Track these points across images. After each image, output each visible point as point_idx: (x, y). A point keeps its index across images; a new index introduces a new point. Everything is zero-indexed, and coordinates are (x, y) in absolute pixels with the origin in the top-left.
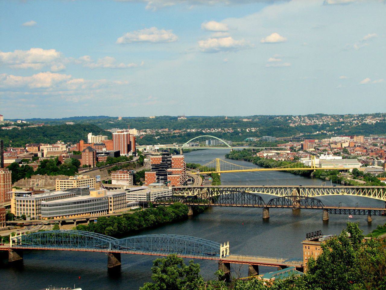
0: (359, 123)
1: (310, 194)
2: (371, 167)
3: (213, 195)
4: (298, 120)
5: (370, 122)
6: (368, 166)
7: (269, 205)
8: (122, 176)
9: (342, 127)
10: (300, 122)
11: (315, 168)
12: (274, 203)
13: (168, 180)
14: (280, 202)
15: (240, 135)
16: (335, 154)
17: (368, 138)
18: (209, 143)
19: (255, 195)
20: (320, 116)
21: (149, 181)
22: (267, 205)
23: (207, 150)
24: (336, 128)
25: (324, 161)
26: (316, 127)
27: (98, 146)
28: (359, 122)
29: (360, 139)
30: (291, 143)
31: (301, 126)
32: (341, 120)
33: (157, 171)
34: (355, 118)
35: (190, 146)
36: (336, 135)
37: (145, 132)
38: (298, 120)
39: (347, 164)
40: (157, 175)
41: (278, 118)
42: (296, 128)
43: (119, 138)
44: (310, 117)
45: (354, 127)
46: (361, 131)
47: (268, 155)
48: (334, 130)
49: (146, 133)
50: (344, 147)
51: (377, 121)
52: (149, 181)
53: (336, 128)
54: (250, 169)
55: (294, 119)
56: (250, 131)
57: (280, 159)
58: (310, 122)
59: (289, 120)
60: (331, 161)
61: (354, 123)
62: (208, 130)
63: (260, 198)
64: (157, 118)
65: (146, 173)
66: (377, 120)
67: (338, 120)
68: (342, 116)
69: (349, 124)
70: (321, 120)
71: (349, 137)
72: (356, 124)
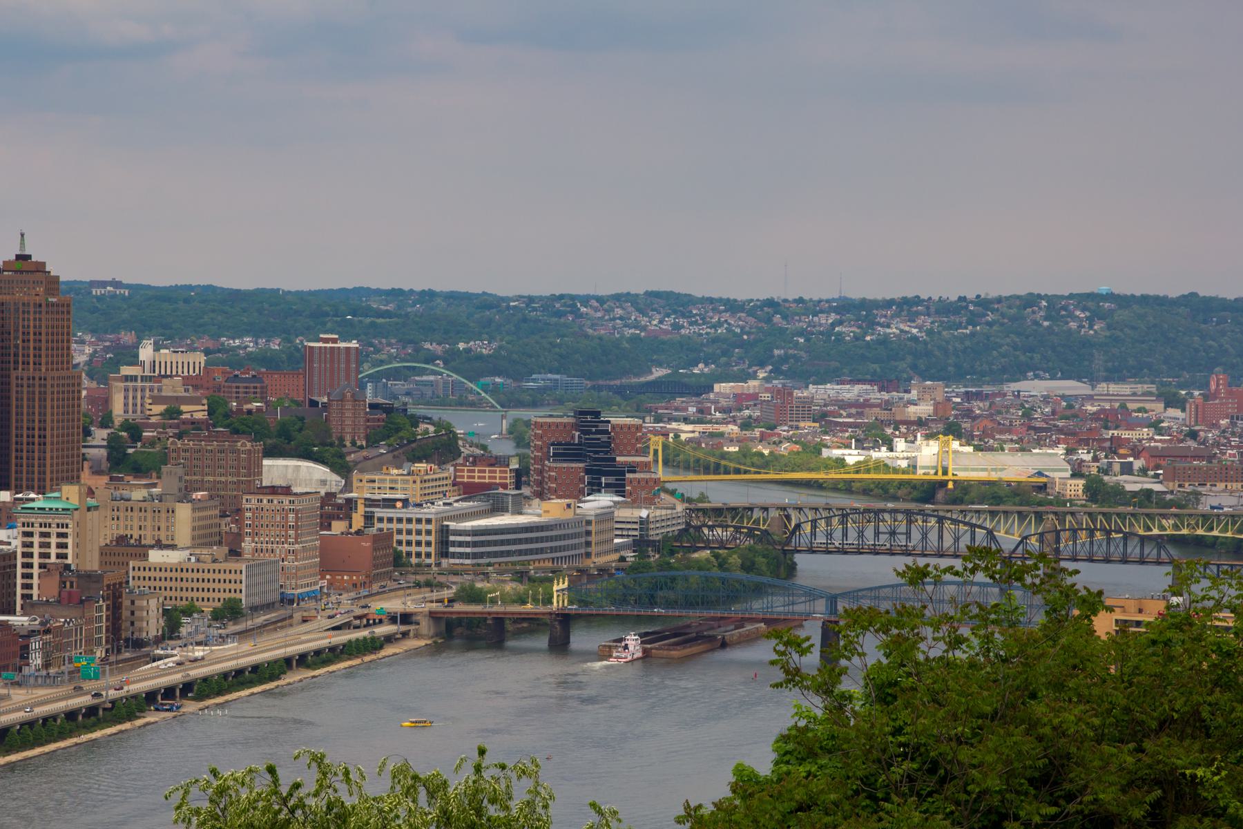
8: (487, 475)
11: (950, 476)
13: (627, 488)
15: (384, 380)
20: (677, 304)
26: (654, 349)
27: (245, 385)
40: (587, 472)
43: (332, 361)
47: (1093, 387)
64: (355, 288)
71: (875, 387)
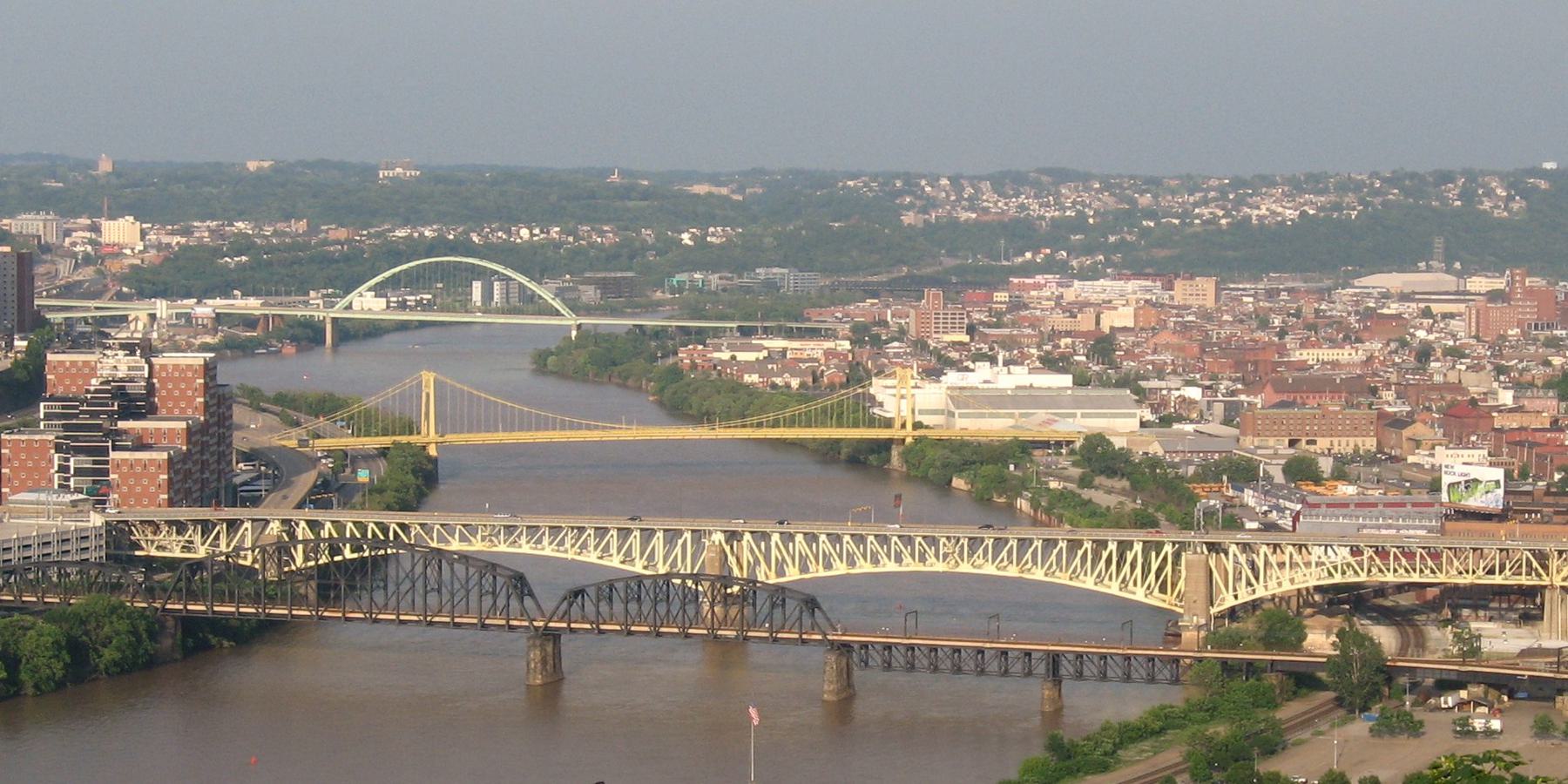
0: (1224, 216)
1: (1166, 576)
2: (1189, 428)
3: (321, 562)
4: (948, 196)
5: (1274, 213)
6: (1176, 426)
7: (561, 620)
9: (1146, 232)
10: (953, 208)
12: (590, 608)
14: (618, 607)
16: (1051, 363)
17: (1241, 286)
18: (488, 294)
19: (494, 566)
21: (17, 478)
22: (166, 603)
23: (427, 333)
24: (1112, 239)
25: (968, 393)
28: (1221, 213)
29: (1197, 292)
30: (873, 304)
31: (954, 224)
32: (1145, 200)
33: (66, 427)
34: (1212, 194)
35: (388, 307)
36: (1109, 270)
37: (187, 232)
38: (948, 196)
39: (1079, 412)
40: (58, 448)
41: (851, 183)
42: (929, 229)
44: (1006, 182)
45: (1196, 235)
46: (1230, 253)
48: (1109, 250)
49: (183, 240)
50: (1112, 328)
51: (1306, 208)
52: (17, 478)
53: (1112, 239)
54: (588, 428)
55: (928, 189)
56: (700, 241)
57: (778, 381)
58: (1000, 204)
59: (901, 193)
60: (1025, 398)
61: (1199, 216)
62: (500, 234)
63: (520, 585)
65: (7, 437)
66: (1305, 204)
67: (1133, 202)
68: (1153, 184)
69: (1176, 221)
70: (1051, 198)
71: (1159, 284)
72: (1205, 223)
